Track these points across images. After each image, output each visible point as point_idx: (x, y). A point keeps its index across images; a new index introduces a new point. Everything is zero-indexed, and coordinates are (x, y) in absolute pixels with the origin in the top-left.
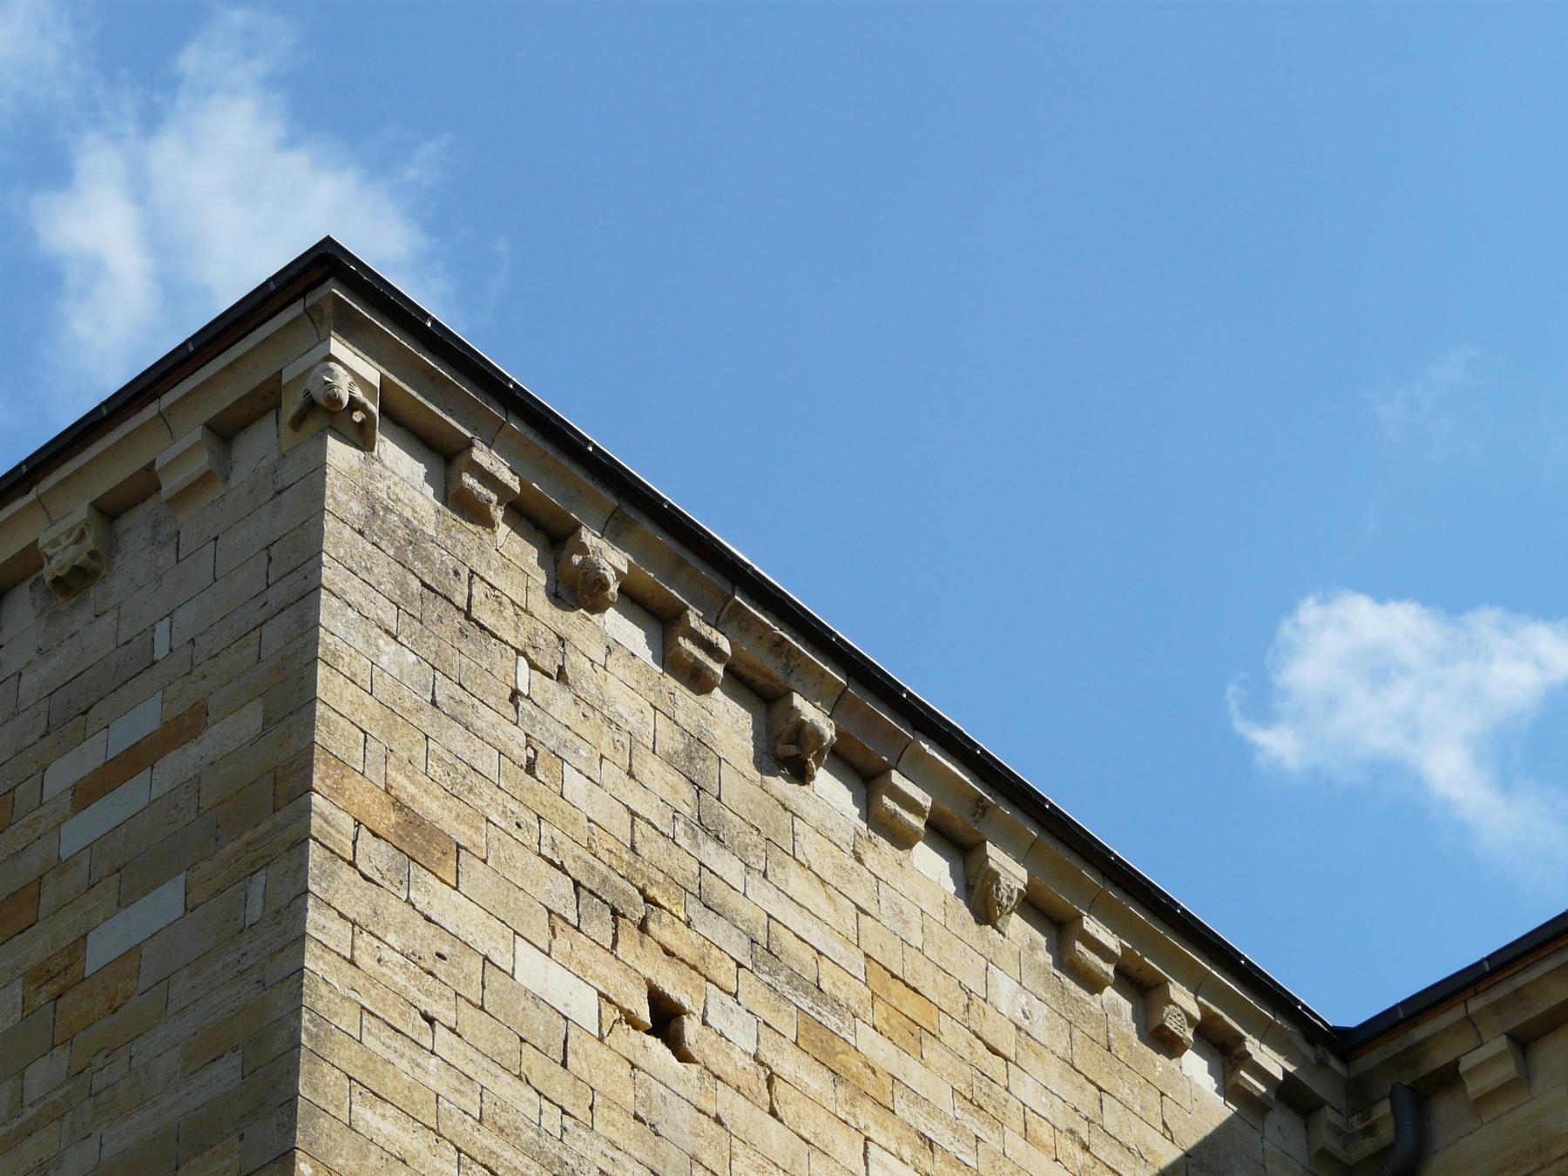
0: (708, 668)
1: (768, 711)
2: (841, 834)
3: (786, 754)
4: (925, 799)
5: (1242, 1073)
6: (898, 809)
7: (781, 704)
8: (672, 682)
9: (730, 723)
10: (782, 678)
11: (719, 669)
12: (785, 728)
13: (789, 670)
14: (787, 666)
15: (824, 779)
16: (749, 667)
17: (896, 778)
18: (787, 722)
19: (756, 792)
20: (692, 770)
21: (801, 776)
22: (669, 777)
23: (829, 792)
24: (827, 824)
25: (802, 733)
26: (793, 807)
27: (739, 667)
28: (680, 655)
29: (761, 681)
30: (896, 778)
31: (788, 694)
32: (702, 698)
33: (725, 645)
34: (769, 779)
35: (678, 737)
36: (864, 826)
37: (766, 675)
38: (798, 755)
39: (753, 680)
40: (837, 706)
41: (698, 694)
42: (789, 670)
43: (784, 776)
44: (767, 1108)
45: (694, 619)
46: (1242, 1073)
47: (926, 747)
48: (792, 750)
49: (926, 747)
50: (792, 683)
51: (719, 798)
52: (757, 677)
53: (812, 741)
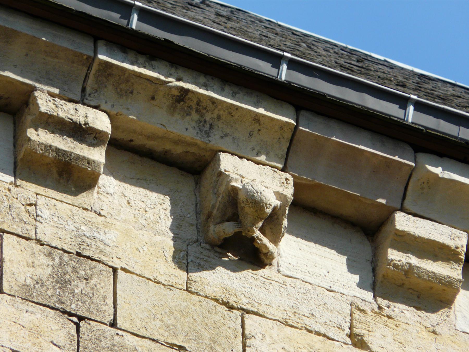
0: (83, 159)
1: (197, 183)
2: (327, 316)
3: (225, 236)
4: (457, 239)
5: (301, 128)
6: (414, 261)
7: (208, 173)
8: (30, 189)
9: (133, 218)
10: (34, 117)
11: (98, 155)
12: (214, 202)
13: (206, 128)
14: (201, 122)
15: (293, 252)
16: (149, 138)
17: (403, 222)
18: (216, 194)
19: (179, 299)
20: (66, 297)
21: (255, 258)
22: (26, 318)
23: (309, 267)
24: (304, 310)
25: (237, 205)
26: (244, 302)
27: (121, 136)
28: (33, 152)
29: (178, 150)
30: (403, 222)
31: (212, 158)
32: (84, 198)
33: (101, 122)
34: (195, 276)
35: (44, 260)
36: (369, 296)
37: (178, 142)
38: (238, 235)
39: (166, 152)
40: (288, 153)
41: (75, 194)
42: (206, 128)
43: (226, 266)
44: (342, 336)
45: (46, 101)
46: (301, 128)
47: (438, 170)
48: (229, 229)
49: (438, 170)
50: (215, 141)
51: (113, 324)
52: (168, 146)
53: (249, 210)
